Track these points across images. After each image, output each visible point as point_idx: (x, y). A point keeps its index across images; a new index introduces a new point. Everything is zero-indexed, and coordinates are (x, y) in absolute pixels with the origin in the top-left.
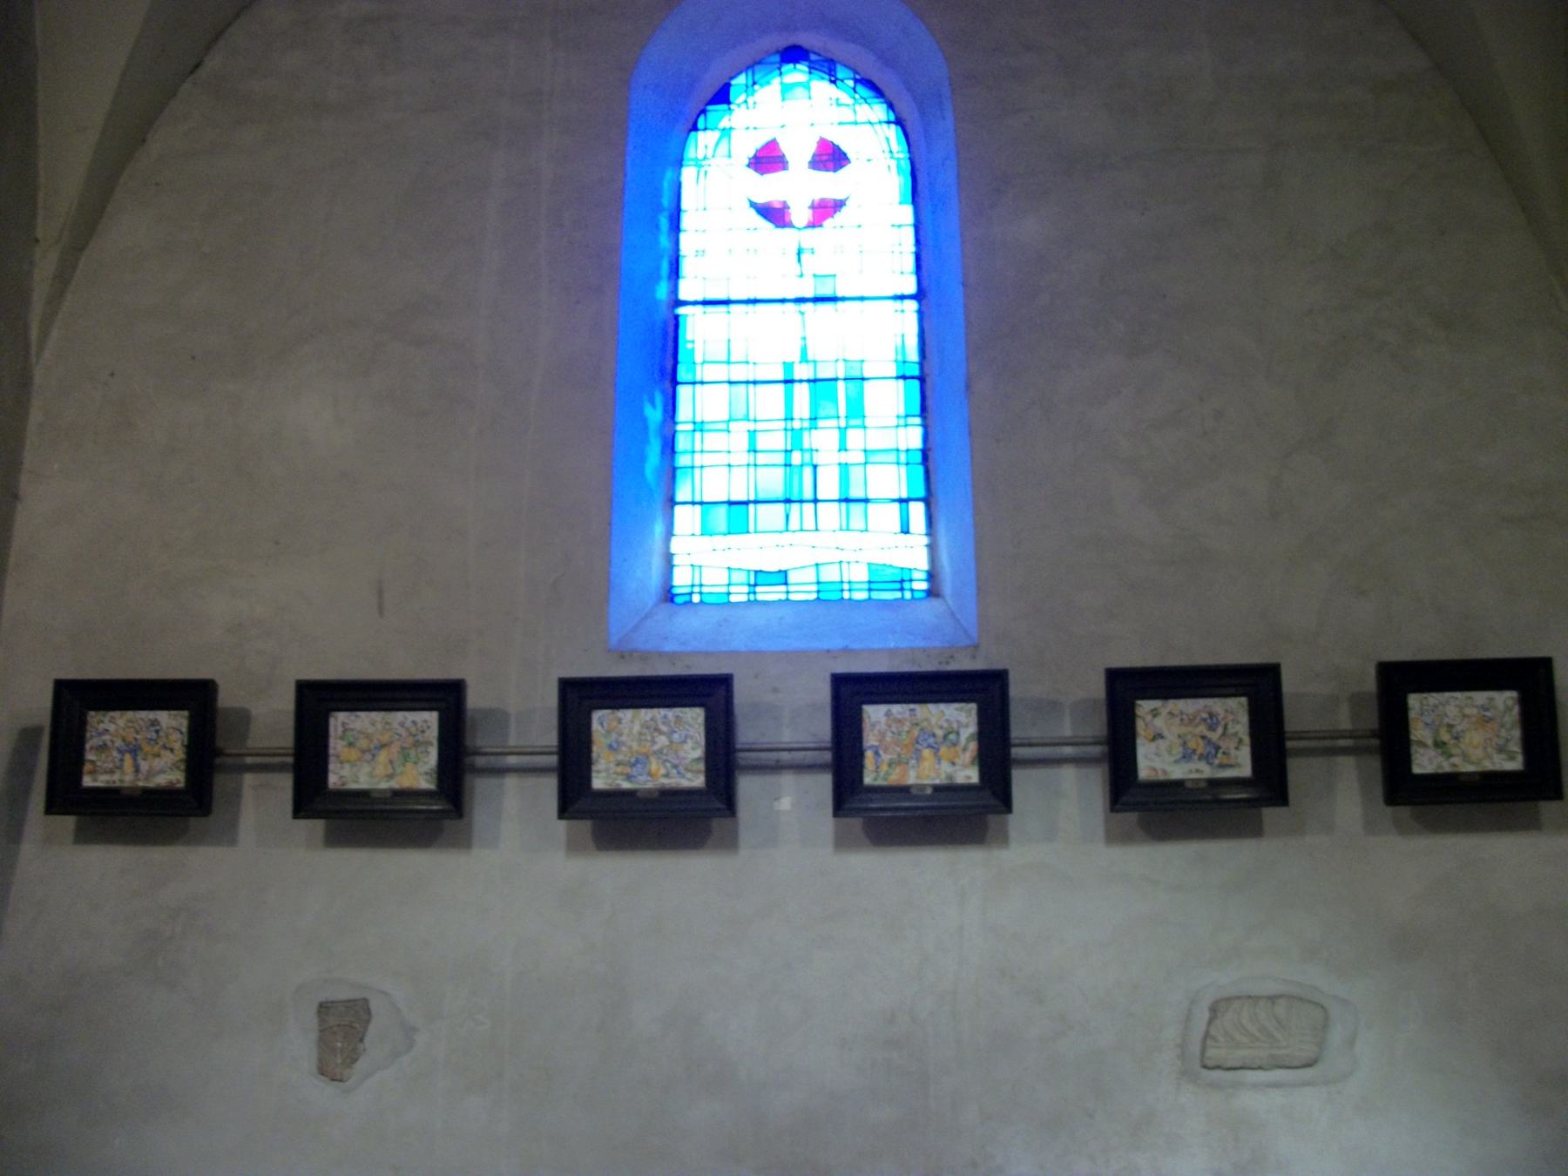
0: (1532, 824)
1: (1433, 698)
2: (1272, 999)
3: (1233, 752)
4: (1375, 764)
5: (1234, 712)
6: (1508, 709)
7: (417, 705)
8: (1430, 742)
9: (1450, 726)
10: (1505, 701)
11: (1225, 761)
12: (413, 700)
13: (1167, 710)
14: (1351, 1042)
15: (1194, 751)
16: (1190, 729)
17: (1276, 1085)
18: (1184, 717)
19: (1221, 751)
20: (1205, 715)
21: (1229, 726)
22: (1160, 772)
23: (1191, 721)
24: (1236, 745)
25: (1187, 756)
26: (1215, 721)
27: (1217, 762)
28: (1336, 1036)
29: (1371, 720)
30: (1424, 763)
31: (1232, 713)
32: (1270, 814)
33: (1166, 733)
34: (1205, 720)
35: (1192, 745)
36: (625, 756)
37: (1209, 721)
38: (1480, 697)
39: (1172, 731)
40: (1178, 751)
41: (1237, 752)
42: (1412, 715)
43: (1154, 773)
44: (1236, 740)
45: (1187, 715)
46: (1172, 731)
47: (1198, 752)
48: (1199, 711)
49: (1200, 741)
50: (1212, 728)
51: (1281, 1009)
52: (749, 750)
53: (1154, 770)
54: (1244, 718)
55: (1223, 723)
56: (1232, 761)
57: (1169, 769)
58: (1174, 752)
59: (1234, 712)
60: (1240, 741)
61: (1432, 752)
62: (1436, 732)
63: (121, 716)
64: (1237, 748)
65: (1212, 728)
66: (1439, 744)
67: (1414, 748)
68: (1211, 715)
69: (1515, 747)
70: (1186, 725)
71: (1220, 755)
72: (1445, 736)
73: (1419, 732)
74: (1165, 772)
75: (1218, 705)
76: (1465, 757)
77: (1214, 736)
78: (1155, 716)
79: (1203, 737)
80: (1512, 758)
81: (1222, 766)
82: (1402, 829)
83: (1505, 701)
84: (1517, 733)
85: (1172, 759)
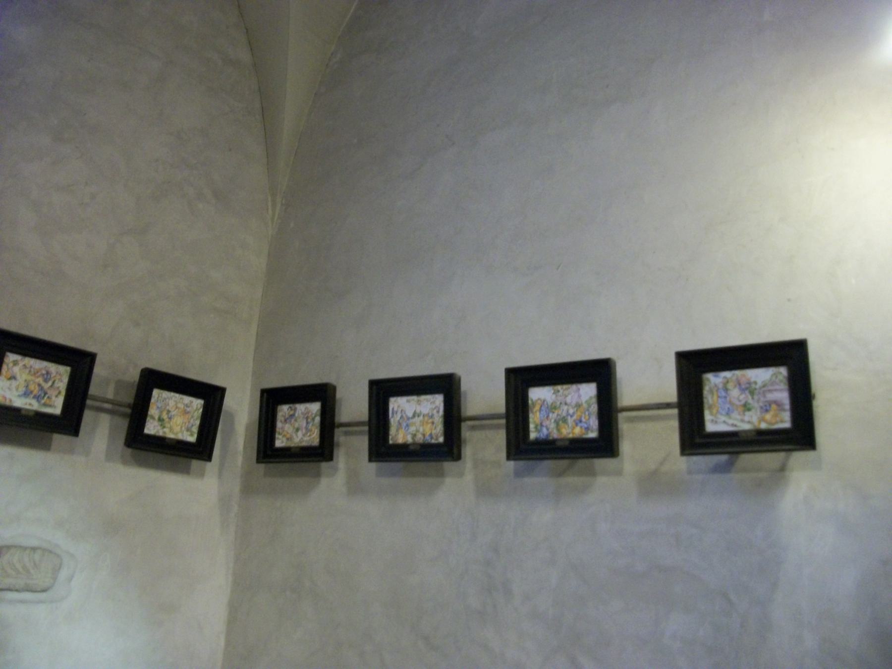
0: (186, 471)
1: (166, 394)
2: (34, 549)
3: (54, 398)
4: (123, 424)
5: (61, 374)
6: (197, 409)
8: (157, 417)
9: (169, 412)
10: (197, 404)
14: (70, 579)
15: (32, 392)
16: (33, 378)
17: (22, 602)
20: (44, 372)
21: (56, 382)
22: (7, 401)
25: (26, 394)
26: (49, 377)
27: (43, 401)
28: (63, 574)
29: (128, 397)
30: (151, 428)
32: (58, 439)
33: (18, 376)
35: (33, 387)
37: (45, 376)
38: (187, 399)
39: (23, 377)
40: (22, 389)
41: (57, 399)
42: (153, 400)
44: (57, 392)
46: (23, 377)
49: (37, 386)
50: (46, 381)
51: (37, 556)
54: (66, 380)
55: (53, 380)
57: (14, 399)
59: (61, 374)
60: (60, 393)
61: (156, 423)
62: (161, 412)
65: (46, 381)
66: (161, 420)
67: (148, 419)
68: (48, 373)
69: (195, 430)
70: (32, 375)
71: (46, 398)
72: (165, 416)
73: (153, 411)
74: (11, 401)
75: (53, 367)
76: (171, 429)
77: (46, 386)
80: (192, 435)
81: (45, 405)
82: (125, 462)
83: (197, 404)
84: (198, 422)
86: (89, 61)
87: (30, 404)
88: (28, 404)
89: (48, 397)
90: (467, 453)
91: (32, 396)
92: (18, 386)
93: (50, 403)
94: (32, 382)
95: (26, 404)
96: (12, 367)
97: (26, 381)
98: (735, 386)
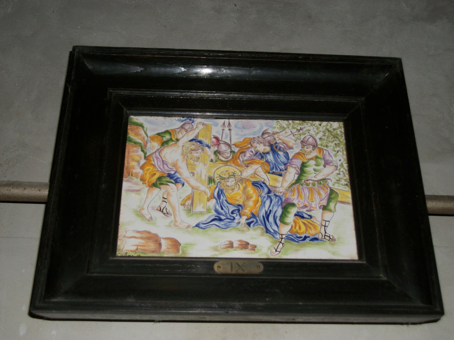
3: (317, 214)
7: (43, 279)
11: (302, 231)
12: (175, 308)
13: (192, 136)
15: (239, 209)
16: (232, 169)
18: (223, 148)
19: (293, 211)
20: (261, 148)
21: (310, 169)
22: (165, 244)
23: (235, 158)
24: (324, 203)
26: (282, 158)
27: (285, 230)
31: (315, 146)
33: (184, 173)
34: (262, 155)
36: (227, 176)
37: (270, 157)
41: (328, 215)
43: (152, 246)
44: (324, 194)
45: (229, 146)
47: (247, 211)
48: (251, 142)
49: (251, 190)
52: (257, 175)
53: (156, 239)
55: (298, 163)
56: (318, 231)
57: (183, 238)
58: (199, 208)
60: (332, 196)
63: (120, 232)
64: (325, 208)
68: (274, 149)
70: (226, 163)
71: (290, 218)
74: (176, 244)
78: (164, 144)
79: (256, 184)
85: (194, 221)
86: (286, 190)
87: (245, 245)
88: (235, 245)
89: (299, 215)
90: (151, 254)
91: (243, 220)
92: (191, 198)
93: (312, 232)
94: (231, 182)
95: (231, 245)
96: (159, 151)
97: (211, 180)
98: (332, 238)
